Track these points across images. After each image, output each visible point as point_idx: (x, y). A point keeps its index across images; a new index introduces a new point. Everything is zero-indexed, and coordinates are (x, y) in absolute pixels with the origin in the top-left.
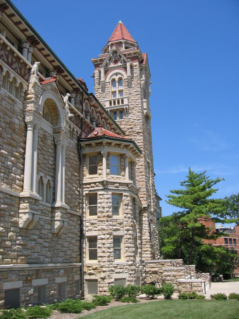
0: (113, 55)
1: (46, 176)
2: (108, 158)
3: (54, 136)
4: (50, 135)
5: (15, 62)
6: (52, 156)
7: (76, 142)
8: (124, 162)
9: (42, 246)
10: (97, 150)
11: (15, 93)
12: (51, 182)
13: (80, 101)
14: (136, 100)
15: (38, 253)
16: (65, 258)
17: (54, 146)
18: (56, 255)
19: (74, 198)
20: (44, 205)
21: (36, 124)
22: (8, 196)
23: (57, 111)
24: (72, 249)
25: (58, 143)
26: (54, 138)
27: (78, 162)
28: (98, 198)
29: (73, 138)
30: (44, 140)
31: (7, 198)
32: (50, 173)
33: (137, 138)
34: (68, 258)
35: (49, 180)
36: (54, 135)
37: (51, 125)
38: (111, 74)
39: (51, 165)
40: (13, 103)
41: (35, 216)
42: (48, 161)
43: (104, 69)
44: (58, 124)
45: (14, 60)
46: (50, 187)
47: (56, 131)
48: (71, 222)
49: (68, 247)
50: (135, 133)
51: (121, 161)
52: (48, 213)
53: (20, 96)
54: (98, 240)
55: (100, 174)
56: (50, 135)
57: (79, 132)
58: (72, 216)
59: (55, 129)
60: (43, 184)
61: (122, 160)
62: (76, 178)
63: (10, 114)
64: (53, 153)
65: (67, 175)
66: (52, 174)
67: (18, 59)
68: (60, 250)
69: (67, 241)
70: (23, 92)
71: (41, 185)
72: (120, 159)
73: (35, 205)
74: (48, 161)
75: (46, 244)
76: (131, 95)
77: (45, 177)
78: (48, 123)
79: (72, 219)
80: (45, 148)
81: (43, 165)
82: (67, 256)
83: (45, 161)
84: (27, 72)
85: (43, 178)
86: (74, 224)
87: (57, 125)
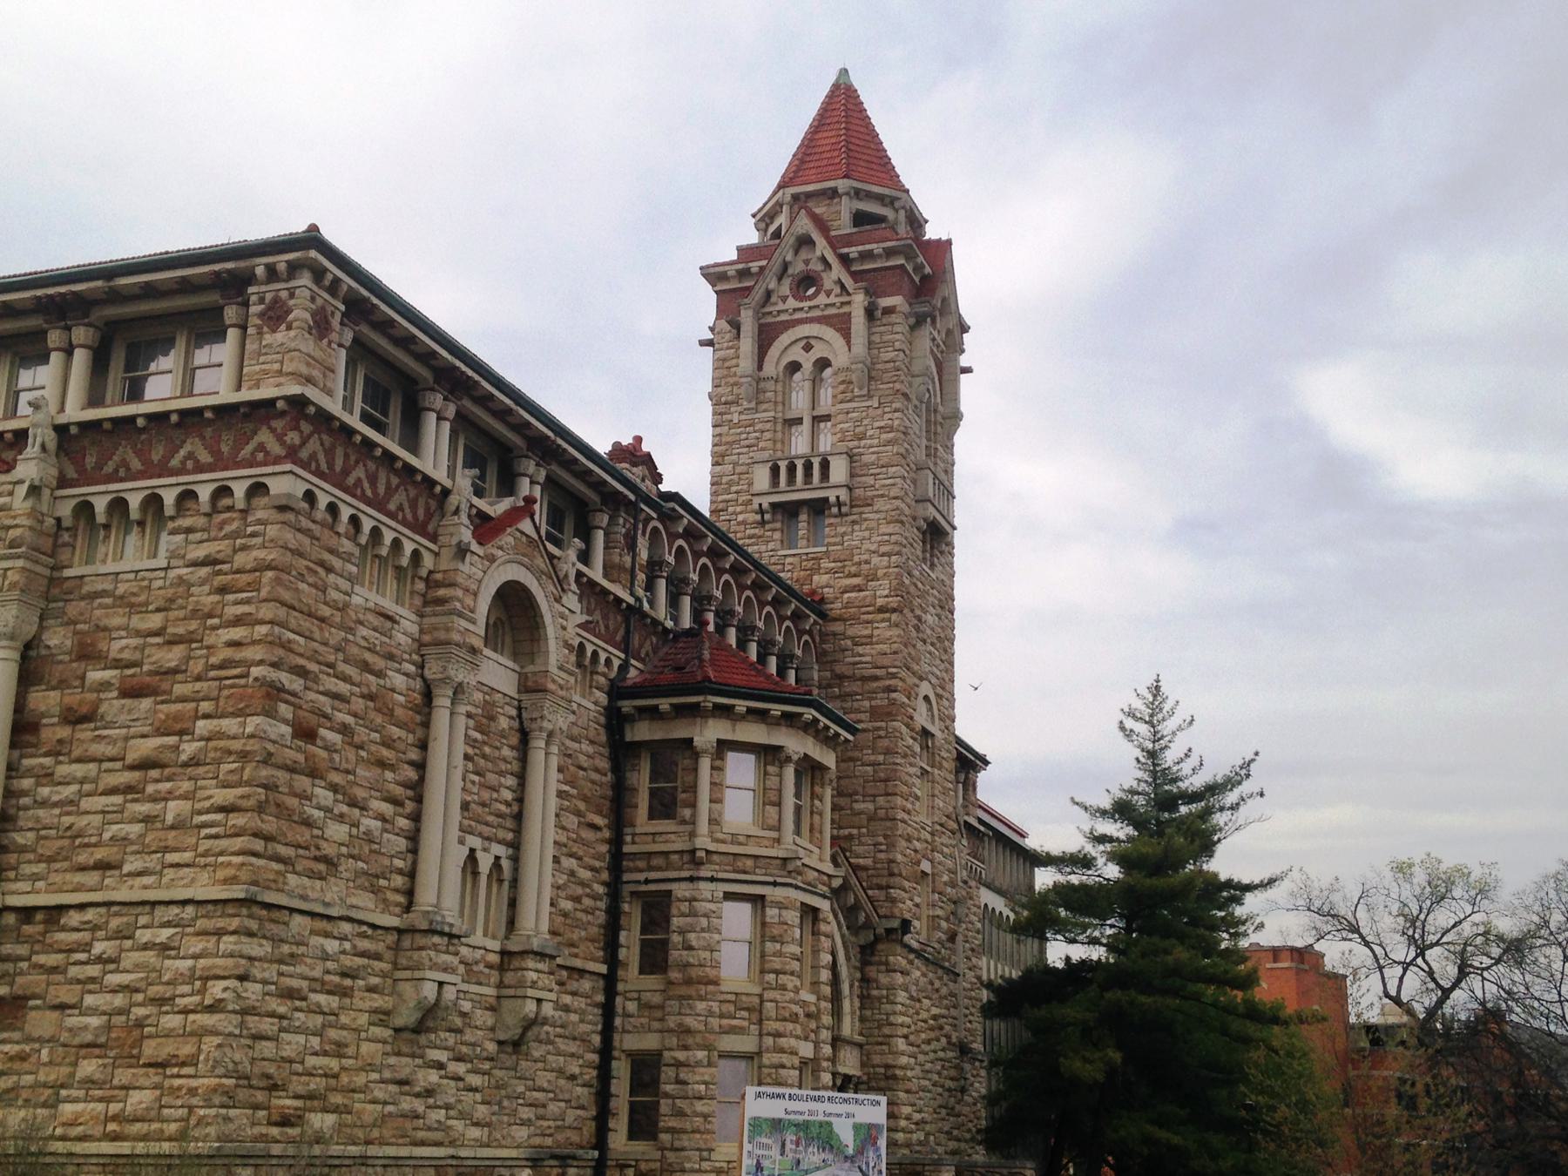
0: (796, 252)
1: (486, 844)
2: (718, 763)
3: (520, 701)
4: (508, 700)
5: (398, 487)
6: (512, 774)
7: (603, 698)
8: (780, 775)
9: (461, 1084)
10: (679, 731)
11: (395, 586)
12: (506, 864)
13: (626, 536)
14: (883, 467)
15: (447, 1109)
16: (539, 1132)
17: (518, 735)
18: (505, 1119)
19: (583, 911)
20: (474, 947)
21: (460, 684)
22: (365, 928)
23: (535, 616)
24: (567, 1097)
25: (534, 726)
26: (519, 709)
27: (609, 774)
28: (674, 911)
29: (591, 687)
30: (484, 721)
31: (363, 935)
32: (501, 834)
33: (876, 632)
34: (548, 1132)
35: (497, 858)
36: (524, 697)
37: (510, 664)
38: (785, 339)
39: (508, 804)
40: (388, 624)
41: (446, 988)
42: (498, 791)
43: (756, 312)
44: (539, 661)
45: (395, 481)
46: (500, 881)
47: (530, 684)
48: (567, 999)
49: (550, 1088)
50: (871, 609)
51: (766, 773)
52: (487, 971)
53: (412, 593)
54: (664, 1068)
55: (684, 822)
56: (508, 700)
57: (616, 663)
58: (576, 977)
59: (527, 678)
60: (476, 874)
61: (770, 769)
62: (599, 835)
63: (379, 663)
64: (515, 762)
65: (563, 828)
66: (510, 836)
67: (410, 470)
68: (521, 1101)
69: (548, 1067)
70: (421, 578)
71: (469, 879)
72: (765, 766)
73: (447, 952)
74: (498, 791)
75: (475, 1080)
76: (863, 443)
77: (485, 850)
78: (502, 659)
79: (573, 985)
80: (487, 750)
81: (479, 810)
82: (545, 1124)
83: (486, 795)
84: (433, 504)
85: (479, 855)
86: (579, 1003)
87: (533, 662)
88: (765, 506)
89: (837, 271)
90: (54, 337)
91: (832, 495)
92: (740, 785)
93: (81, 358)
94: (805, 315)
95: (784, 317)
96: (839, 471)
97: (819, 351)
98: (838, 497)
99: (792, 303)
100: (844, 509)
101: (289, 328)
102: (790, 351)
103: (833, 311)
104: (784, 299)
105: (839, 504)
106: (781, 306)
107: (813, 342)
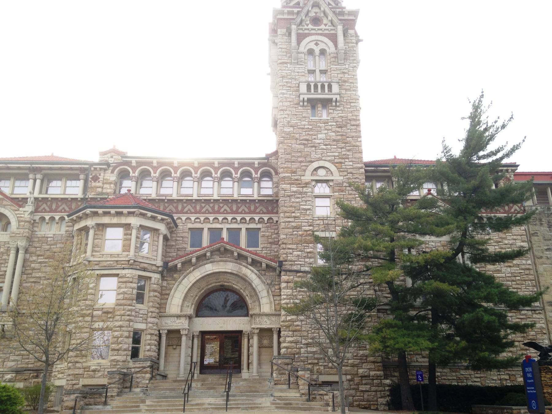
38: (308, 39)
58: (101, 228)
88: (306, 99)
89: (331, 16)
90: (31, 176)
91: (334, 97)
92: (110, 289)
93: (38, 182)
94: (315, 32)
95: (307, 32)
96: (335, 88)
97: (322, 46)
98: (336, 99)
99: (310, 26)
100: (338, 104)
101: (99, 182)
102: (310, 44)
103: (327, 32)
104: (307, 25)
105: (336, 101)
106: (306, 27)
107: (319, 42)
